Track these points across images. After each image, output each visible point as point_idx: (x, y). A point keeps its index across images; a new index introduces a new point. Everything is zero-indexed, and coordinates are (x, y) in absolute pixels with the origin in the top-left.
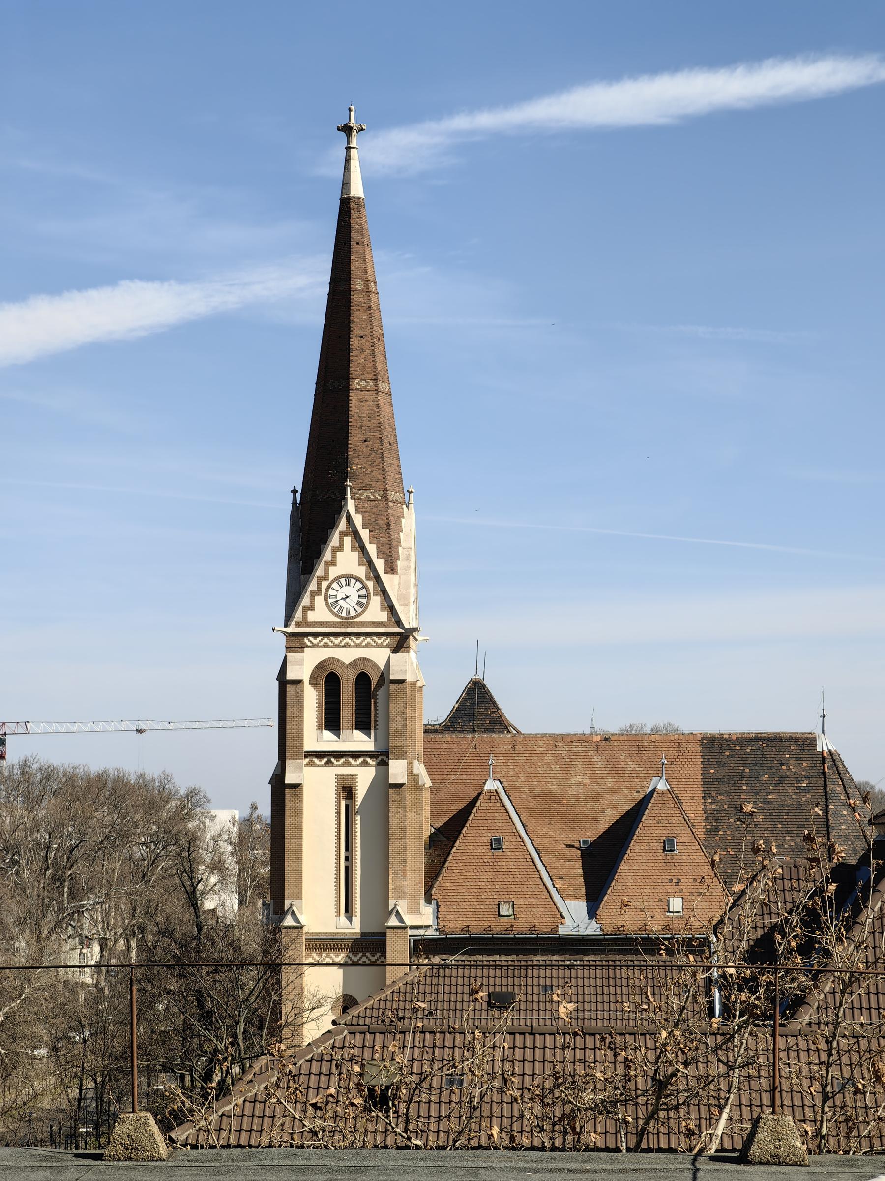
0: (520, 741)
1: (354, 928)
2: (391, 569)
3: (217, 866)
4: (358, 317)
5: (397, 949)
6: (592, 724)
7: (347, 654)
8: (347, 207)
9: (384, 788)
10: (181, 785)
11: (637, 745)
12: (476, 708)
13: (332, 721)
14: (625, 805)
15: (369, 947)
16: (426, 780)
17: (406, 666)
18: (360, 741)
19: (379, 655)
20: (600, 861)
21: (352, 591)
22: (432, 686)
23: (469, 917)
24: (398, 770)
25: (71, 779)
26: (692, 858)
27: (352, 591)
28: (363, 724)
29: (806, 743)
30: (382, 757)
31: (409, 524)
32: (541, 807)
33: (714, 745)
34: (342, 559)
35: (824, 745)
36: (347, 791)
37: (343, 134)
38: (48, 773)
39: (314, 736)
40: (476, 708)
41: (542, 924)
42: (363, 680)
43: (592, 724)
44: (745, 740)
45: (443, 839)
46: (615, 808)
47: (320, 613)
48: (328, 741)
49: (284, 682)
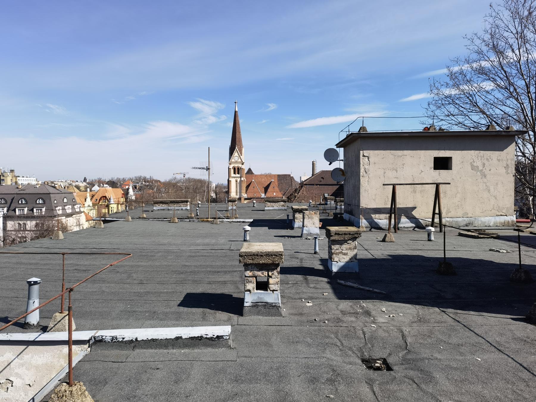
0: (256, 175)
1: (238, 197)
4: (237, 125)
5: (242, 199)
6: (203, 168)
7: (236, 165)
8: (235, 112)
9: (241, 181)
11: (270, 176)
12: (250, 171)
13: (235, 173)
14: (269, 183)
17: (243, 167)
18: (239, 176)
19: (240, 165)
20: (266, 189)
21: (237, 158)
22: (245, 168)
23: (251, 196)
24: (242, 179)
26: (277, 189)
27: (237, 158)
28: (238, 173)
29: (290, 175)
30: (241, 177)
31: (243, 150)
32: (259, 183)
33: (279, 176)
34: (236, 154)
35: (291, 176)
36: (237, 181)
39: (232, 175)
40: (250, 171)
41: (259, 196)
42: (238, 168)
43: (203, 168)
44: (282, 175)
45: (248, 187)
47: (233, 160)
48: (234, 175)
49: (229, 169)
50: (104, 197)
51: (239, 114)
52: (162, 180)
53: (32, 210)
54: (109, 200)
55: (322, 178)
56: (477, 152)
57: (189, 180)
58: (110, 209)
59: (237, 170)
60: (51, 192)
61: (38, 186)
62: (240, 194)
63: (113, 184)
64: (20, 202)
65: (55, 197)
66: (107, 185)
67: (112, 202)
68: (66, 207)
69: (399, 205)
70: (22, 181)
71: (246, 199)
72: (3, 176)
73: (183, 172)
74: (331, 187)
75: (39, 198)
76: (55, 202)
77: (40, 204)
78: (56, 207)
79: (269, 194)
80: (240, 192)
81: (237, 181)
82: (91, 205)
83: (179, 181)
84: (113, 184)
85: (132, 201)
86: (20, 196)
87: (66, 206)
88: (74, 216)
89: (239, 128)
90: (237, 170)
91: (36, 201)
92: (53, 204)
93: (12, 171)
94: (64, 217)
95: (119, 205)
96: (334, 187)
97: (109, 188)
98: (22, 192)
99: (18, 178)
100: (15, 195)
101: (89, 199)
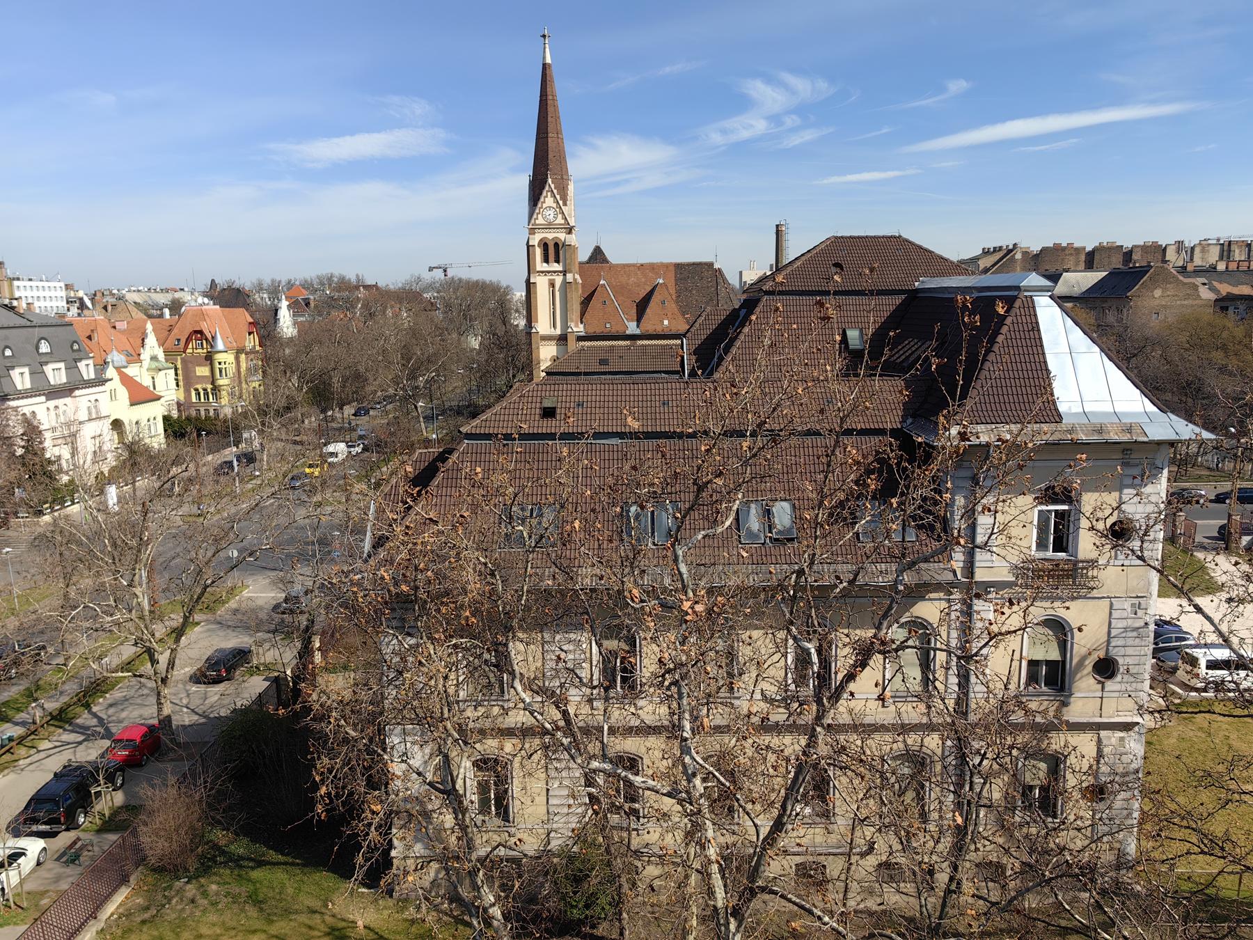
1: (558, 332)
2: (565, 204)
3: (517, 311)
4: (550, 109)
5: (571, 340)
7: (550, 236)
8: (545, 66)
9: (565, 284)
10: (504, 284)
11: (653, 268)
12: (597, 255)
13: (546, 260)
15: (562, 339)
17: (572, 239)
19: (562, 236)
20: (642, 307)
21: (551, 212)
24: (570, 277)
25: (468, 282)
26: (672, 306)
27: (551, 212)
28: (557, 261)
29: (711, 265)
30: (564, 273)
31: (571, 187)
33: (679, 267)
34: (548, 201)
35: (716, 266)
36: (552, 285)
38: (460, 280)
39: (540, 265)
40: (597, 255)
42: (556, 245)
44: (689, 265)
45: (586, 302)
47: (540, 221)
48: (545, 267)
49: (528, 247)
50: (196, 332)
51: (555, 73)
54: (211, 342)
55: (837, 265)
57: (455, 285)
59: (554, 251)
62: (565, 325)
65: (6, 338)
67: (220, 345)
68: (48, 369)
71: (580, 339)
73: (441, 262)
76: (8, 353)
79: (649, 325)
81: (552, 285)
82: (161, 356)
84: (230, 297)
87: (47, 363)
88: (77, 393)
89: (557, 118)
90: (554, 251)
91: (37, 348)
94: (43, 398)
95: (243, 356)
96: (885, 300)
99: (16, 283)
101: (151, 340)
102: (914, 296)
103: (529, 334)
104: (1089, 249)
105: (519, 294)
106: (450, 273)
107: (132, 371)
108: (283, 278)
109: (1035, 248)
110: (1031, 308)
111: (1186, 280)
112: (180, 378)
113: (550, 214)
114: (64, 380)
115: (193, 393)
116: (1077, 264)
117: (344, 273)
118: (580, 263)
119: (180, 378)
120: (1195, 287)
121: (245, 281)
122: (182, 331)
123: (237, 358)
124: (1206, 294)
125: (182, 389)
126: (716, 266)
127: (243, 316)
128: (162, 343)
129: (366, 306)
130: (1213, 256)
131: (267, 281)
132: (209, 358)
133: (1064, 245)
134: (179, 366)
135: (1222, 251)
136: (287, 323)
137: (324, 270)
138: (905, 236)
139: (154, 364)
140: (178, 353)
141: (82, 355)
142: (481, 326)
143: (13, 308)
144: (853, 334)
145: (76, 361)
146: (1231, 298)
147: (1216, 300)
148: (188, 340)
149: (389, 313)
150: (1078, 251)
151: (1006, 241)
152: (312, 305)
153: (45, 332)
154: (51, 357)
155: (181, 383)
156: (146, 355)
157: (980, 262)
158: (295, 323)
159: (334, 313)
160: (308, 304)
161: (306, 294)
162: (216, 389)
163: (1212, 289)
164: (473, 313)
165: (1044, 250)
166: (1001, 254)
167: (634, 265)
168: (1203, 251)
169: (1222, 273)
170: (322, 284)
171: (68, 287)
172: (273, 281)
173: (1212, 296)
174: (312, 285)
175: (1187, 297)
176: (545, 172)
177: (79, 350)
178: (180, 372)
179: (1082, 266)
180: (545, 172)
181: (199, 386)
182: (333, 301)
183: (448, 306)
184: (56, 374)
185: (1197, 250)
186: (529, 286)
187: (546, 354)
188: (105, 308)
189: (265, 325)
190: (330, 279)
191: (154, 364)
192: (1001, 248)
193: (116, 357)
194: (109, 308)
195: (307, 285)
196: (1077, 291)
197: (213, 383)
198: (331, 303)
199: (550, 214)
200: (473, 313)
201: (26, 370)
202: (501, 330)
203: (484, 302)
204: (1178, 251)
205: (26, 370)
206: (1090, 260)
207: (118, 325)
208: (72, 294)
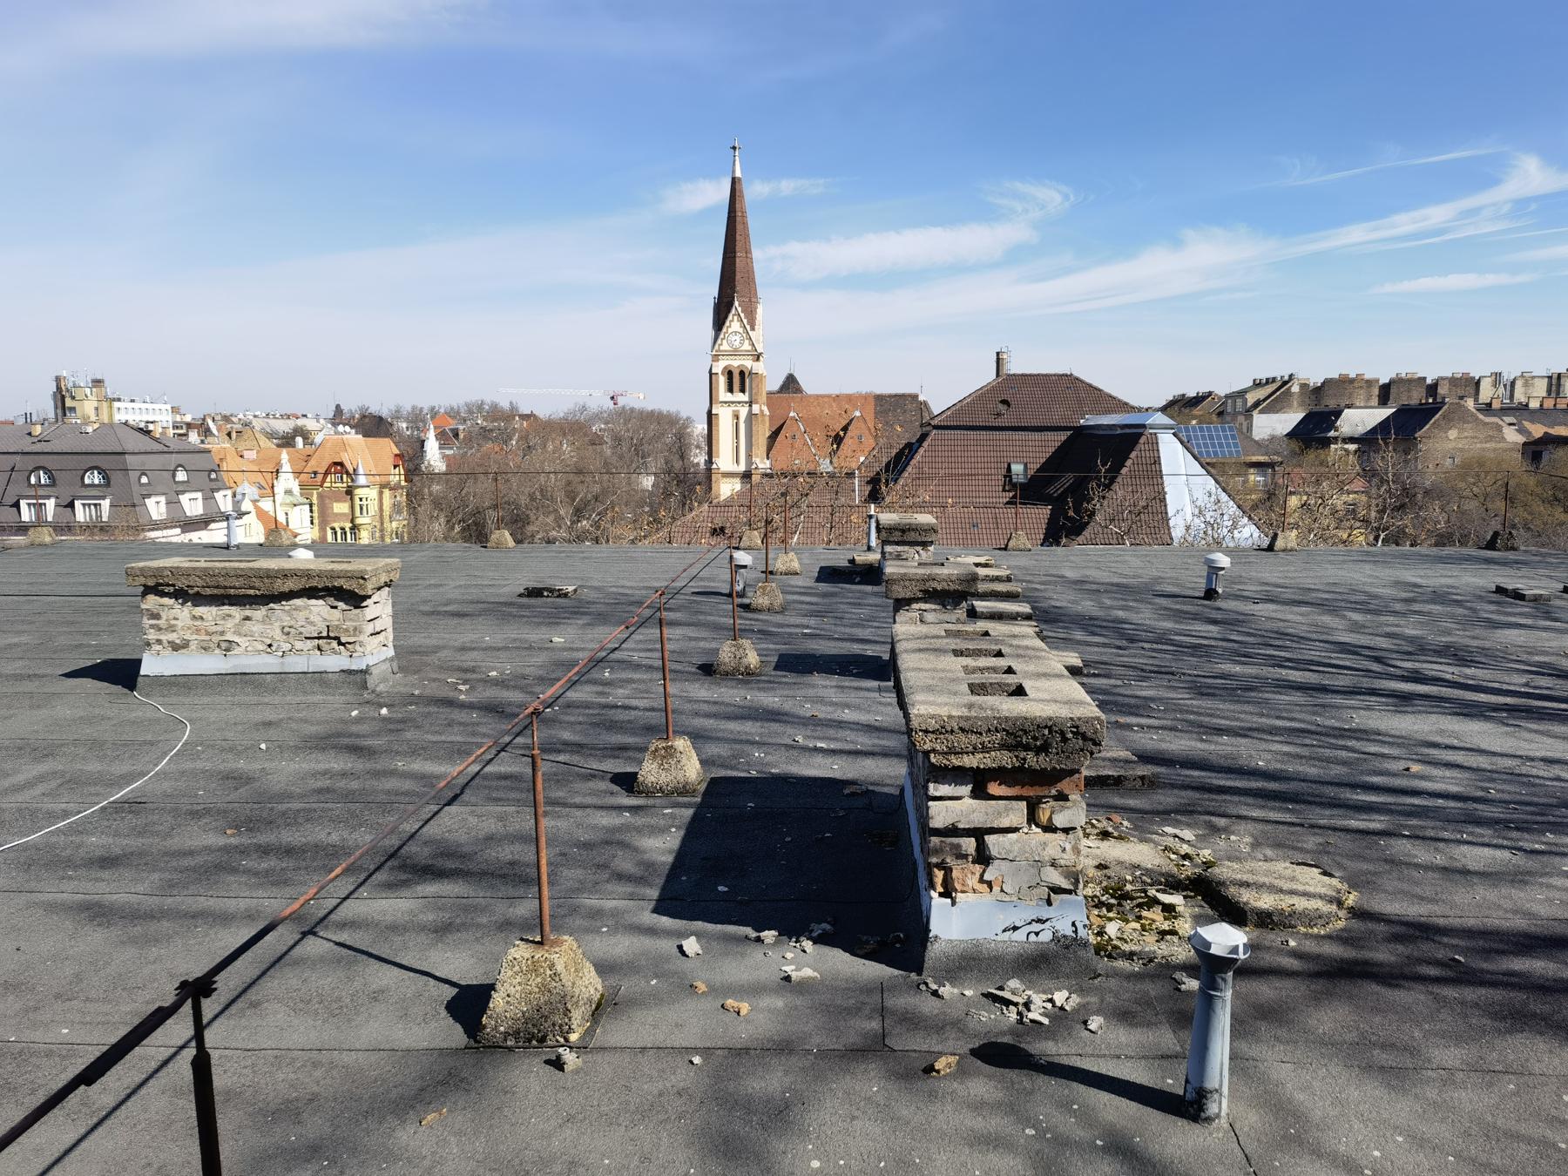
1: (742, 468)
2: (753, 329)
3: (698, 447)
4: (739, 227)
5: (756, 478)
7: (735, 363)
8: (734, 181)
9: (751, 415)
10: (684, 415)
12: (791, 384)
13: (731, 390)
15: (746, 476)
16: (767, 412)
17: (759, 367)
18: (745, 397)
19: (748, 363)
21: (738, 338)
23: (782, 464)
25: (641, 412)
27: (738, 338)
28: (743, 390)
29: (915, 397)
32: (811, 422)
33: (879, 398)
34: (733, 325)
35: (921, 398)
37: (1546, 456)
38: (632, 410)
39: (723, 395)
40: (791, 384)
42: (742, 373)
44: (891, 396)
46: (1409, 397)
47: (725, 347)
48: (729, 397)
49: (711, 374)
50: (336, 464)
52: (543, 412)
53: (71, 505)
55: (1005, 402)
56: (218, 1116)
57: (627, 415)
58: (357, 502)
59: (739, 380)
60: (129, 447)
61: (90, 429)
63: (372, 426)
64: (33, 480)
66: (347, 428)
69: (986, 837)
70: (128, 413)
72: (73, 398)
74: (1037, 435)
75: (92, 468)
77: (92, 485)
78: (145, 496)
80: (749, 456)
82: (296, 490)
83: (597, 417)
84: (372, 426)
85: (433, 476)
86: (32, 462)
87: (183, 492)
88: (213, 526)
89: (747, 237)
90: (739, 380)
91: (83, 478)
92: (135, 488)
93: (98, 383)
94: (178, 530)
96: (1050, 435)
97: (353, 437)
98: (38, 447)
99: (116, 404)
100: (18, 458)
102: (1080, 433)
103: (709, 470)
104: (1384, 380)
105: (700, 427)
106: (621, 401)
107: (266, 505)
108: (425, 404)
109: (1316, 379)
110: (1154, 444)
111: (1488, 420)
112: (316, 515)
113: (736, 340)
114: (201, 511)
115: (329, 532)
116: (1369, 398)
117: (497, 400)
118: (770, 393)
119: (316, 515)
120: (1499, 428)
121: (381, 405)
122: (320, 463)
123: (381, 493)
124: (1513, 436)
125: (316, 528)
126: (921, 398)
127: (388, 448)
128: (297, 474)
129: (524, 438)
130: (1540, 389)
131: (407, 407)
132: (350, 492)
133: (1353, 375)
134: (315, 501)
135: (1550, 385)
136: (434, 457)
137: (474, 397)
138: (1076, 374)
139: (289, 499)
140: (314, 486)
141: (219, 484)
142: (655, 463)
143: (148, 432)
144: (1017, 468)
145: (213, 490)
146: (1548, 440)
147: (1525, 444)
148: (326, 473)
149: (550, 447)
150: (1370, 383)
151: (1281, 372)
152: (461, 436)
153: (182, 458)
154: (186, 487)
155: (316, 521)
156: (280, 488)
157: (1248, 396)
158: (444, 456)
159: (489, 445)
160: (456, 435)
161: (453, 424)
162: (355, 528)
163: (1521, 431)
164: (646, 448)
165: (1326, 382)
166: (1274, 387)
167: (829, 396)
168: (1526, 384)
169: (1534, 411)
170: (470, 412)
171: (175, 410)
172: (414, 408)
173: (1521, 439)
174: (458, 413)
175: (1490, 438)
176: (731, 292)
177: (216, 480)
178: (315, 508)
179: (1375, 401)
180: (731, 292)
181: (336, 525)
182: (489, 431)
183: (618, 440)
184: (193, 505)
185: (1519, 384)
186: (711, 417)
187: (727, 489)
188: (229, 435)
189: (411, 458)
190: (480, 407)
191: (289, 499)
192: (1274, 380)
193: (248, 489)
194: (234, 435)
195: (453, 413)
196: (1361, 430)
197: (352, 521)
198: (485, 433)
199: (736, 340)
200: (646, 448)
201: (162, 499)
202: (678, 465)
203: (659, 436)
204: (1495, 384)
205: (162, 499)
206: (1385, 394)
207: (246, 454)
208: (178, 418)
